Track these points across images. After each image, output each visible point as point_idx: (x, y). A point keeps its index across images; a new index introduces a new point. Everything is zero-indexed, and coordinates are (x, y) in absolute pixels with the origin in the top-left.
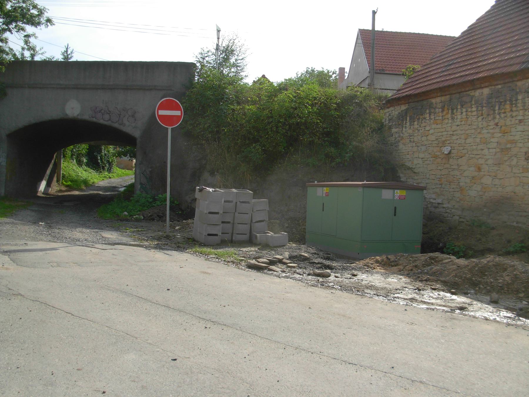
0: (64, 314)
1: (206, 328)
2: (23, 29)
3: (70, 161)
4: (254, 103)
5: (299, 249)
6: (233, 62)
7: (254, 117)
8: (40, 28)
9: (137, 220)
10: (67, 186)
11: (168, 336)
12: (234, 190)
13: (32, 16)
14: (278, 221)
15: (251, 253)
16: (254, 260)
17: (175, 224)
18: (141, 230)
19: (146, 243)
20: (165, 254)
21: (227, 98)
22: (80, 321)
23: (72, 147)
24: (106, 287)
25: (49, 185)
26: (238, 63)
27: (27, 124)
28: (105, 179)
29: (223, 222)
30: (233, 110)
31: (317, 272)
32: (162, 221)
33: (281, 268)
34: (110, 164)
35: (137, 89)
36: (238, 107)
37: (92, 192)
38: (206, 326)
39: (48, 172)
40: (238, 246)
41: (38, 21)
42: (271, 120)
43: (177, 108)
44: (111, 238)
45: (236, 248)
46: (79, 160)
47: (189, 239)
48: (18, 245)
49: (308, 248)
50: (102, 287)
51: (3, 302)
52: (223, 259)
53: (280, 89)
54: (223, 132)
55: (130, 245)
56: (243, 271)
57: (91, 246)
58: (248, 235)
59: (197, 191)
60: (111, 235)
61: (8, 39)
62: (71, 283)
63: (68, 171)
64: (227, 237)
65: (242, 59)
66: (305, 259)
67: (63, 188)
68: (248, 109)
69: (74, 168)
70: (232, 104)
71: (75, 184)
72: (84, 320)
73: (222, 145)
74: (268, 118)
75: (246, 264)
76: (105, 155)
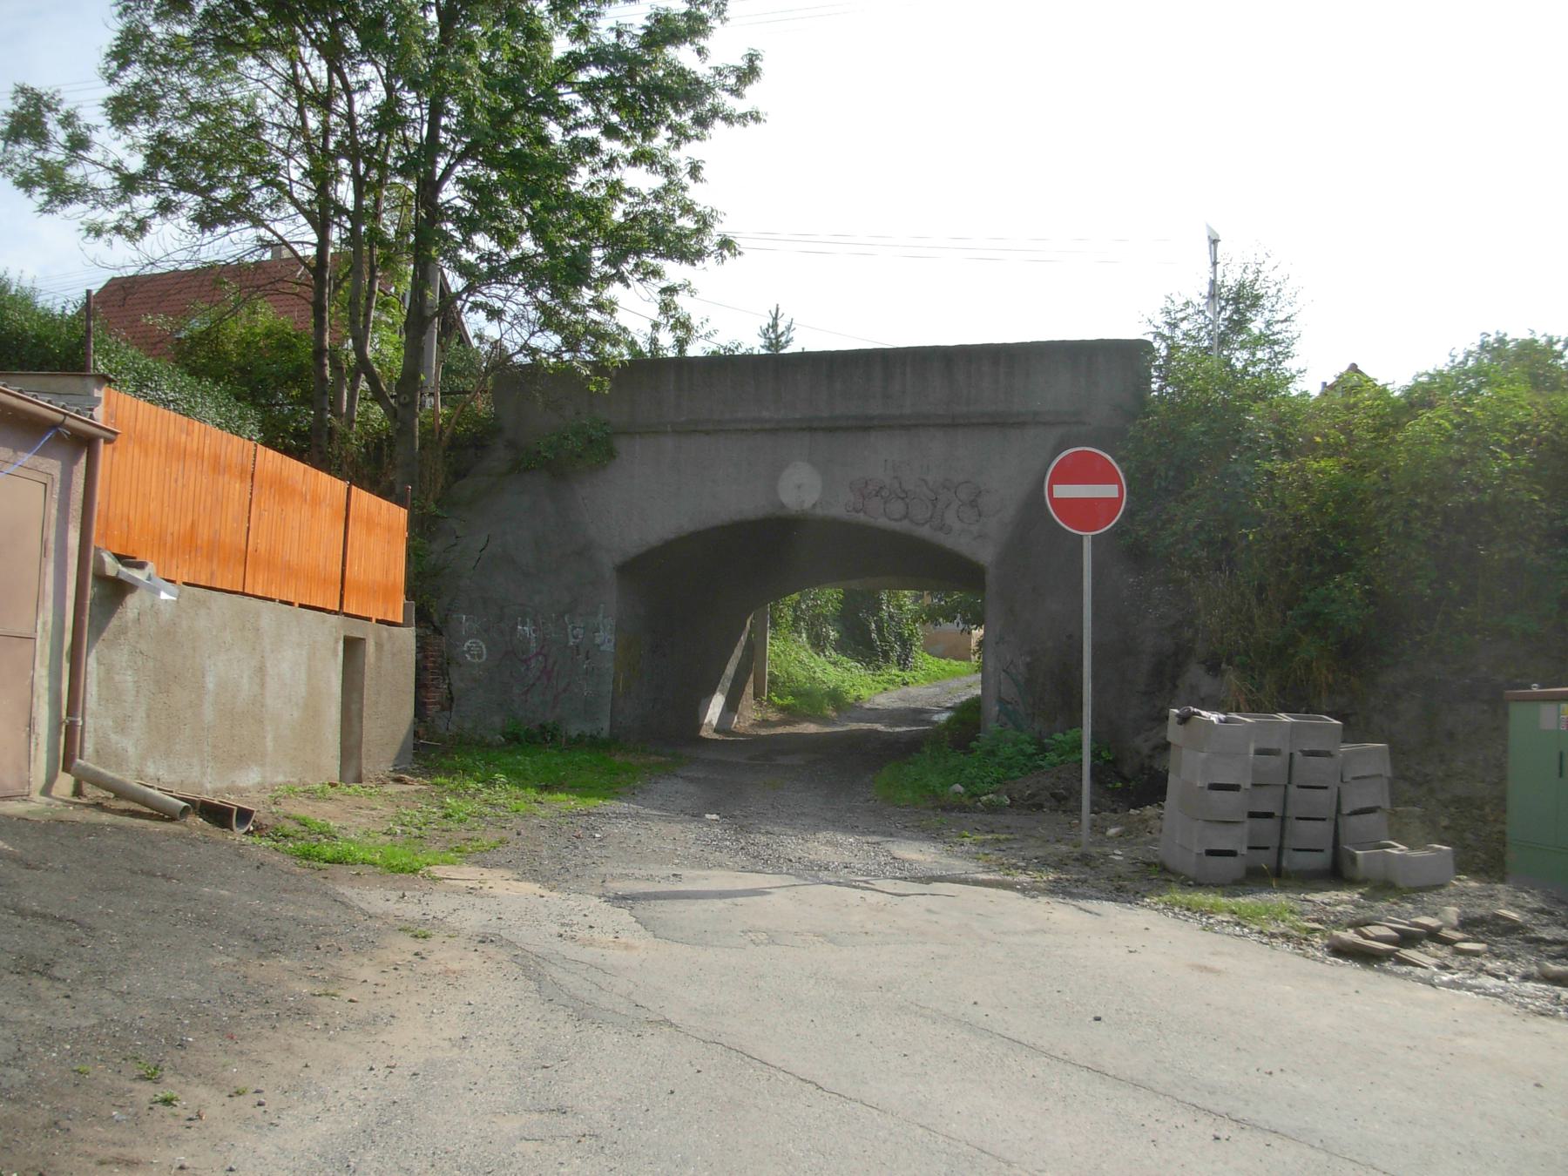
0: (795, 1084)
1: (1217, 1138)
2: (656, 273)
3: (791, 637)
4: (1333, 450)
5: (1491, 896)
6: (1261, 332)
7: (1336, 495)
8: (703, 266)
9: (992, 809)
10: (782, 709)
11: (1104, 1162)
12: (1284, 718)
13: (681, 236)
14: (1417, 810)
15: (1339, 908)
16: (1351, 931)
17: (1104, 820)
18: (1007, 840)
19: (1023, 878)
20: (1081, 909)
21: (1250, 440)
22: (840, 1107)
23: (796, 596)
24: (913, 1007)
25: (731, 706)
26: (1273, 334)
27: (672, 536)
28: (891, 687)
29: (1252, 815)
30: (1271, 475)
31: (1552, 971)
32: (1064, 812)
33: (1436, 957)
34: (906, 644)
35: (984, 424)
36: (1286, 466)
37: (854, 726)
38: (1217, 1134)
39: (730, 669)
40: (1300, 887)
41: (698, 247)
42: (1387, 500)
43: (1108, 477)
44: (917, 862)
45: (1292, 892)
46: (817, 631)
47: (1149, 864)
48: (654, 880)
49: (1519, 894)
50: (900, 1008)
51: (621, 1042)
52: (1257, 928)
53: (1412, 405)
54: (1244, 543)
55: (977, 883)
56: (1320, 964)
57: (862, 884)
58: (1329, 852)
59: (1173, 721)
60: (919, 853)
61: (616, 304)
62: (812, 994)
63: (785, 665)
64: (1265, 860)
65: (1286, 320)
66: (1512, 928)
67: (773, 716)
68: (1317, 472)
69: (803, 656)
70: (1266, 455)
71: (808, 701)
72: (853, 1104)
73: (1242, 580)
74: (1379, 494)
75: (1326, 942)
76: (891, 617)
